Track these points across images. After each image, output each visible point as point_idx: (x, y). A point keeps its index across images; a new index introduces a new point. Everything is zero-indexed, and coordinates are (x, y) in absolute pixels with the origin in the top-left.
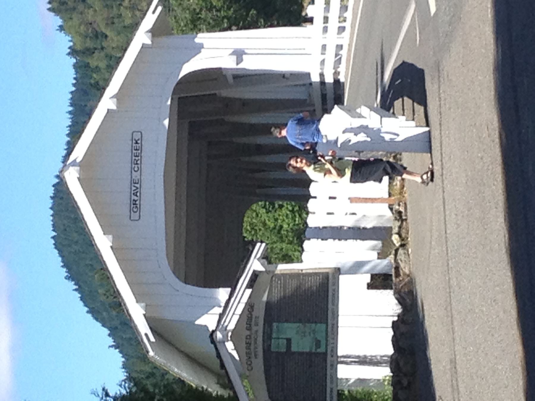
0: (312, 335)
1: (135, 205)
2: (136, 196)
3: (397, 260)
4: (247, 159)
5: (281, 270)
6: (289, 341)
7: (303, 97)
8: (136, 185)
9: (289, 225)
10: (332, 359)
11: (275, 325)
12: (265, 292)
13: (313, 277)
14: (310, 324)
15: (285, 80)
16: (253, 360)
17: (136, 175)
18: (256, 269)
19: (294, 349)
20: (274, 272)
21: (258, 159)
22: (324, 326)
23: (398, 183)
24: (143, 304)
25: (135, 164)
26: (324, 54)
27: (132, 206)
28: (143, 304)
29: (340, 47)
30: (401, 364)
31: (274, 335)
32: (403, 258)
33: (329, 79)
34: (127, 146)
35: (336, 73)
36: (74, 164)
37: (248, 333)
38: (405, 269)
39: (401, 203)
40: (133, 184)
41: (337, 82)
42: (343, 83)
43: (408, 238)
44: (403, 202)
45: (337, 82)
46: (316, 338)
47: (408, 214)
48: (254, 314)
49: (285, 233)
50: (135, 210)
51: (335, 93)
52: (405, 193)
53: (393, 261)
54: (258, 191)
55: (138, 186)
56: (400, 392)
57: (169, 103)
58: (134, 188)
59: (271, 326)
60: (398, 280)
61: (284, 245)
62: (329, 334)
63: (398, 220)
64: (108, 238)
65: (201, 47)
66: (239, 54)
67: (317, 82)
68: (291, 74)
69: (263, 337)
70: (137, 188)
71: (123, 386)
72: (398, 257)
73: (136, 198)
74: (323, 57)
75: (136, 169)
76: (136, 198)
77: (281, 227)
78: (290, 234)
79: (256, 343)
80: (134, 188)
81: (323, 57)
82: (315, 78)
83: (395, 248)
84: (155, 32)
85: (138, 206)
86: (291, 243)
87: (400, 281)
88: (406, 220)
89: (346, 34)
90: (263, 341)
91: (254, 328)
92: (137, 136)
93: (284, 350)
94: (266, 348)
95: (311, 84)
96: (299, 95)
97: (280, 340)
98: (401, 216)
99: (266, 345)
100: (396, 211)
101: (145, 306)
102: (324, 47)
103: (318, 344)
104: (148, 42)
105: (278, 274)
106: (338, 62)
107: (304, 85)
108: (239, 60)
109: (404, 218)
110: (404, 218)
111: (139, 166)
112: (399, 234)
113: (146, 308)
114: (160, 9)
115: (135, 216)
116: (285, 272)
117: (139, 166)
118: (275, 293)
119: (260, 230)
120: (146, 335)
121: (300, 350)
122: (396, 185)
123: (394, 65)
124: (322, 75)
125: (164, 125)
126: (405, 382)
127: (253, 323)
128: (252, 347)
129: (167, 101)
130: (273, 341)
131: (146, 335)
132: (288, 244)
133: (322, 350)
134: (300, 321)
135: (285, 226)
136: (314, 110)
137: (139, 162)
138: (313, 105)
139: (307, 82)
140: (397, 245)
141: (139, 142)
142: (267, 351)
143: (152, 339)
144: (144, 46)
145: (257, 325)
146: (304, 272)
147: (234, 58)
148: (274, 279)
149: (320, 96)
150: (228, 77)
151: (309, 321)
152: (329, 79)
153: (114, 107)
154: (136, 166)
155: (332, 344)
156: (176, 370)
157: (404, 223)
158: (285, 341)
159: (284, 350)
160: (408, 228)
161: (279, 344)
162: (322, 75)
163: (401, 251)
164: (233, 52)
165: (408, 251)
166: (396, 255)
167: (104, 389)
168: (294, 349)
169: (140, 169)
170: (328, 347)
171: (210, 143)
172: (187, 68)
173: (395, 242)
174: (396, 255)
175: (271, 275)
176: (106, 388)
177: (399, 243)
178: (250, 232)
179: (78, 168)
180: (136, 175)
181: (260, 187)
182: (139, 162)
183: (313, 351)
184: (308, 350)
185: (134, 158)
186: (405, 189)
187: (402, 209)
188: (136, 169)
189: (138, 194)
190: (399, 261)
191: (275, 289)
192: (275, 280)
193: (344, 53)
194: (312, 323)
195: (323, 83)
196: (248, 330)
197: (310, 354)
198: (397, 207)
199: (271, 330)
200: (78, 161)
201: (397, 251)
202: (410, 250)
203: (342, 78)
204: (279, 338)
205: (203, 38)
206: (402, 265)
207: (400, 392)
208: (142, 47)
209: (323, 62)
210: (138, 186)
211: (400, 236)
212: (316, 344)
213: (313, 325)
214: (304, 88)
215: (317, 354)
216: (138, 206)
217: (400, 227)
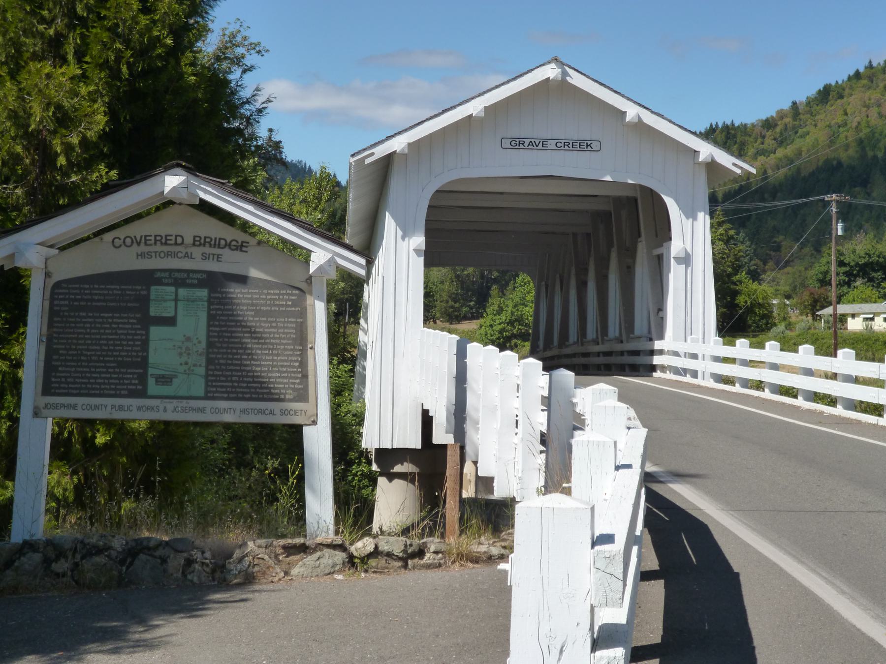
0: (181, 369)
1: (518, 143)
2: (529, 145)
3: (321, 550)
4: (573, 272)
5: (313, 305)
6: (171, 321)
7: (637, 332)
8: (541, 143)
9: (528, 312)
10: (135, 409)
11: (204, 293)
12: (266, 273)
13: (299, 370)
14: (204, 364)
15: (656, 311)
16: (135, 249)
17: (551, 144)
18: (313, 257)
19: (155, 332)
20: (311, 294)
21: (573, 283)
22: (201, 392)
23: (483, 549)
24: (406, 151)
25: (564, 143)
26: (685, 357)
27: (518, 140)
28: (406, 151)
29: (695, 374)
30: (100, 559)
31: (182, 292)
32: (324, 561)
33: (657, 360)
34: (585, 135)
35: (663, 368)
36: (565, 74)
37: (189, 240)
38: (302, 566)
39: (440, 555)
40: (541, 141)
41: (653, 368)
42: (652, 376)
43: (366, 571)
44: (442, 561)
45: (653, 368)
46: (176, 377)
47: (417, 572)
48: (226, 253)
49: (521, 309)
50: (513, 143)
51: (640, 365)
52: (461, 565)
53: (319, 540)
54: (543, 283)
55: (540, 146)
56: (37, 557)
57: (630, 181)
58: (537, 142)
59: (201, 284)
60: (280, 551)
61: (510, 308)
62: (184, 403)
63: (405, 551)
64: (481, 111)
65: (695, 218)
66: (686, 260)
67: (654, 347)
68: (662, 318)
69: (179, 271)
70: (537, 146)
71: (256, 92)
72: (327, 552)
73: (526, 144)
74: (682, 355)
75: (559, 145)
76: (526, 144)
77: (526, 306)
78: (519, 313)
79: (168, 254)
80: (537, 142)
81: (682, 355)
82: (658, 345)
83: (347, 544)
84: (712, 166)
85: (517, 147)
86: (512, 314)
87: (276, 556)
88: (405, 566)
89: (712, 384)
90: (171, 271)
91: (197, 252)
92: (595, 146)
93: (153, 311)
94: (158, 275)
95: (651, 340)
96: (640, 326)
97: (173, 303)
98: (413, 556)
99: (163, 275)
100: (425, 544)
101: (404, 153)
102: (694, 356)
103: (164, 380)
104: (701, 158)
105: (305, 300)
106: (677, 371)
107: (650, 332)
108: (679, 260)
109: (410, 562)
110: (410, 562)
111: (562, 148)
112: (376, 553)
113: (403, 155)
114: (738, 171)
115: (506, 143)
116: (309, 316)
117: (562, 148)
118: (268, 294)
119: (524, 289)
120: (735, 165)
121: (152, 346)
122: (480, 543)
123: (725, 529)
124: (661, 352)
125: (605, 175)
126: (61, 566)
127: (207, 250)
128: (159, 248)
129: (632, 180)
130: (172, 289)
131: (373, 154)
132: (512, 311)
133: (153, 387)
134: (210, 345)
135: (527, 309)
136: (622, 342)
137: (521, 146)
138: (628, 342)
139: (654, 335)
140: (352, 549)
141: (589, 148)
142: (148, 278)
143: (368, 161)
144: (696, 153)
145: (205, 257)
146: (310, 352)
147: (683, 255)
148: (298, 292)
149: (639, 349)
150: (661, 248)
151: (209, 362)
152: (657, 360)
153: (628, 118)
154: (562, 145)
155: (165, 408)
156: (351, 196)
157: (400, 564)
158: (172, 314)
159: (153, 311)
160: (389, 573)
161: (166, 301)
162: (661, 352)
163: (340, 556)
164: (689, 254)
165: (339, 572)
166: (332, 546)
167: (252, 67)
168: (155, 332)
169: (558, 148)
170: (159, 401)
171: (588, 235)
172: (670, 202)
173: (359, 544)
174: (332, 546)
175: (303, 286)
176: (254, 70)
177: (355, 554)
178: (523, 282)
179: (560, 77)
180: (551, 144)
181: (547, 286)
182: (566, 148)
183: (151, 371)
184: (151, 360)
185: (571, 142)
186: (469, 564)
187: (429, 558)
188: (559, 145)
189: (531, 147)
190: (318, 554)
191: (275, 294)
192: (292, 295)
193: (688, 379)
194: (207, 369)
195: (652, 353)
196: (194, 241)
197: (144, 363)
198: (432, 549)
199: (192, 286)
200: (568, 78)
201: (342, 547)
202: (340, 577)
203: (657, 374)
204: (176, 300)
205: (703, 220)
206: (310, 559)
207: (37, 557)
208: (695, 151)
209: (676, 354)
210: (540, 146)
211: (371, 555)
212: (163, 376)
213: (202, 371)
214: (645, 331)
215: (143, 379)
216: (517, 147)
217: (389, 555)
